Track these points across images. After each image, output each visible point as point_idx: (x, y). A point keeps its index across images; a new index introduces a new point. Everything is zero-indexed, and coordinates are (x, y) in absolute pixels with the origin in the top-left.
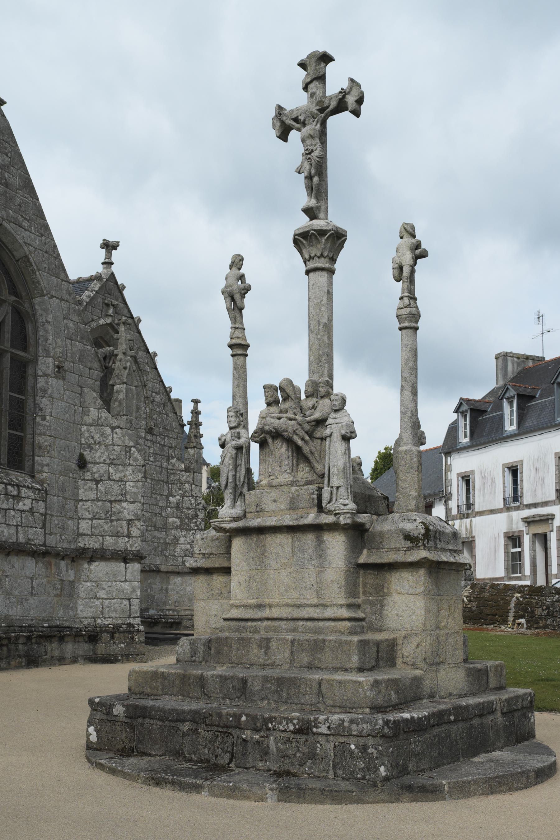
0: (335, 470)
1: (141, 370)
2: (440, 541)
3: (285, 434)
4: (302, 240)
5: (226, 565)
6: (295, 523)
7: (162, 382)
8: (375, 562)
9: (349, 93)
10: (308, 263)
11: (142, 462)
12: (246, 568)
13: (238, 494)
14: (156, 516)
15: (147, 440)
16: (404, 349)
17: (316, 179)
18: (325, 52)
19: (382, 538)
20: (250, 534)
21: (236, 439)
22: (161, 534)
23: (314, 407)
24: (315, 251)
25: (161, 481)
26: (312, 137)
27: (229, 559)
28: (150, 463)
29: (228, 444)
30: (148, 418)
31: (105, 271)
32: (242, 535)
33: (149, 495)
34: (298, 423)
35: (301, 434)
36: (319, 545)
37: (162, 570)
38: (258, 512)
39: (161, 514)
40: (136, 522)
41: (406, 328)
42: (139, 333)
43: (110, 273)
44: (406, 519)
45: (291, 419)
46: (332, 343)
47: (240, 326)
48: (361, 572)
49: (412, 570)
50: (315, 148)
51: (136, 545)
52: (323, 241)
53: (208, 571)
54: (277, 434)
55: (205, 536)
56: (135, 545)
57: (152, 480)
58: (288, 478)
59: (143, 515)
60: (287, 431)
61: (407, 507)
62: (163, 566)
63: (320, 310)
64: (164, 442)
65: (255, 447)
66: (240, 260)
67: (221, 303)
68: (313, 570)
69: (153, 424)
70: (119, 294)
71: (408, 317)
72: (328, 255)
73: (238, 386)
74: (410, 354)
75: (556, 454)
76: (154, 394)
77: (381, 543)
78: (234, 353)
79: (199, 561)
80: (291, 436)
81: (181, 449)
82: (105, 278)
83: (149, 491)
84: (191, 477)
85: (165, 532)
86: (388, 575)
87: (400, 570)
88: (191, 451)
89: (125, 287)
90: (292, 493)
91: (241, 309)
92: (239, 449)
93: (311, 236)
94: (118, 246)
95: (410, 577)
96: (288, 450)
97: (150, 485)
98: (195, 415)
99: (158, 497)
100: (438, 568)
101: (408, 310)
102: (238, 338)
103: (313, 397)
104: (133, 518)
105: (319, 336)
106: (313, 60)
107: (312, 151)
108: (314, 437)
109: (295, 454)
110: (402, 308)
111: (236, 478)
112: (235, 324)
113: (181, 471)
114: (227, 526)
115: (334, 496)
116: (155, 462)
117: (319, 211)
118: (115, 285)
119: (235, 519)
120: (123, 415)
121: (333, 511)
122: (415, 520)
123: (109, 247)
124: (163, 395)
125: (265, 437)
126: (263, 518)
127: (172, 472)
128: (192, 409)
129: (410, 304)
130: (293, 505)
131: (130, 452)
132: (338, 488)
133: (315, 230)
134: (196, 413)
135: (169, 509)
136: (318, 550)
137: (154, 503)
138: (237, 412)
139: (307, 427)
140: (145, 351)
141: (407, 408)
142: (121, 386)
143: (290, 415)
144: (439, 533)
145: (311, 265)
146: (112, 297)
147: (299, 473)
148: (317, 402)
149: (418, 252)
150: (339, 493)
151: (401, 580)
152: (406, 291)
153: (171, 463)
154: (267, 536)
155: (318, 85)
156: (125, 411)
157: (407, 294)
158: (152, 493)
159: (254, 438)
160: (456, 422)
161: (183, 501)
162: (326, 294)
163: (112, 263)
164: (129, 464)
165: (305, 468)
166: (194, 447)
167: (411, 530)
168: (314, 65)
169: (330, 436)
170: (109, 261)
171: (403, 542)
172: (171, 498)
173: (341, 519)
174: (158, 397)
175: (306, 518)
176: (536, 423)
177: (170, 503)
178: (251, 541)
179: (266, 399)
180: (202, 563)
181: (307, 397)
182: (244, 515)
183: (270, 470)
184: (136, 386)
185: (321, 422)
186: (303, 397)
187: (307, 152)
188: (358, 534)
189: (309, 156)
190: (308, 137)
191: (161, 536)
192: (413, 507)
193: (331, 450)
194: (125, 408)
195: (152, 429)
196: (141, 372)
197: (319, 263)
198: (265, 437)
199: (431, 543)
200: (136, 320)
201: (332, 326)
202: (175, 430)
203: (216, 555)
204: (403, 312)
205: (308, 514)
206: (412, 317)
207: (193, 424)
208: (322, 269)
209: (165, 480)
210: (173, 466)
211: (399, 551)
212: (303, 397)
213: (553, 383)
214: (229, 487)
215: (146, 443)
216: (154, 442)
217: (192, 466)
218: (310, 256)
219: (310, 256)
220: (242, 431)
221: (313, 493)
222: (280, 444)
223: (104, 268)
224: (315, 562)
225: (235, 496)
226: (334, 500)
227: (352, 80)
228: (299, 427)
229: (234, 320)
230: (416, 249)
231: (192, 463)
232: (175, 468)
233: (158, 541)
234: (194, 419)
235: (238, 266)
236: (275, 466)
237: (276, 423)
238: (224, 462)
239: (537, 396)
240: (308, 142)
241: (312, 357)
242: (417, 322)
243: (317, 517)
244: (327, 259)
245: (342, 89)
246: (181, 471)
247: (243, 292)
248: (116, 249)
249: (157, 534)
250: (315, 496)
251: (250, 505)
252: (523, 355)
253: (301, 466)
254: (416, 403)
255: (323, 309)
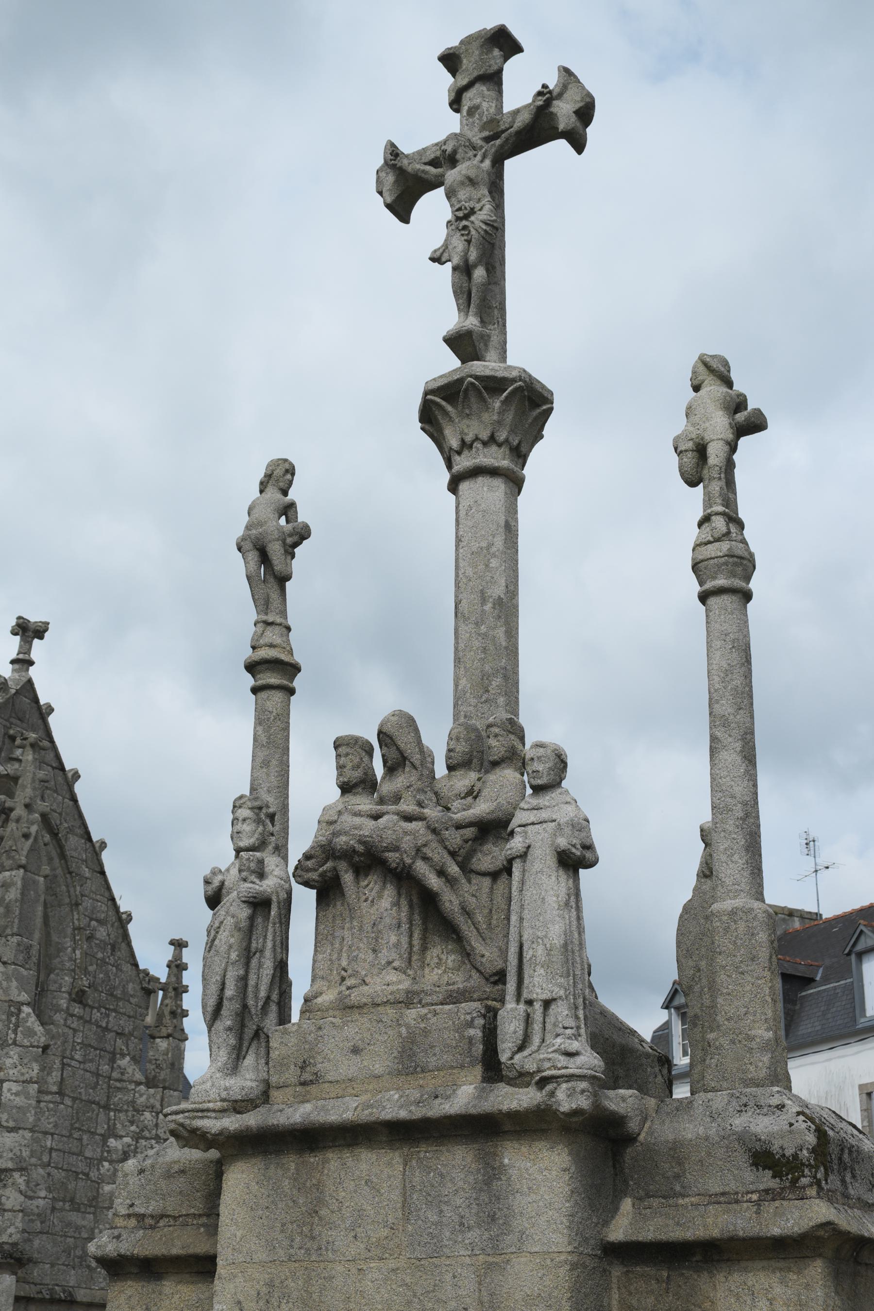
0: (540, 951)
1: (70, 873)
2: (854, 1177)
3: (392, 857)
4: (443, 403)
5: (201, 1248)
6: (418, 1113)
7: (113, 900)
8: (663, 1237)
9: (560, 96)
10: (456, 458)
11: (43, 1039)
12: (261, 1256)
13: (249, 1032)
14: (77, 1178)
15: (72, 1015)
16: (718, 643)
17: (479, 273)
18: (503, 26)
19: (680, 1164)
20: (279, 1152)
21: (253, 878)
22: (84, 1219)
23: (472, 793)
24: (476, 428)
25: (94, 1102)
26: (471, 182)
27: (213, 1230)
28: (73, 1063)
29: (228, 893)
30: (77, 971)
31: (16, 676)
32: (253, 1155)
33: (64, 1132)
34: (428, 827)
35: (436, 858)
36: (488, 1183)
37: (79, 1299)
38: (303, 1084)
39: (87, 1175)
40: (16, 1175)
41: (720, 591)
42: (74, 799)
43: (24, 680)
44: (751, 1104)
45: (408, 818)
46: (517, 649)
47: (279, 620)
48: (617, 1272)
49: (782, 1264)
50: (478, 206)
51: (12, 1230)
52: (497, 404)
53: (149, 1268)
54: (369, 860)
55: (149, 1162)
56: (9, 1231)
57: (74, 1099)
58: (396, 982)
59: (49, 1174)
60: (396, 849)
61: (744, 1072)
62: (82, 1292)
63: (487, 566)
64: (107, 1023)
65: (305, 900)
66: (287, 471)
67: (236, 568)
68: (468, 1260)
69: (86, 983)
70: (40, 721)
71: (726, 564)
72: (507, 441)
73: (266, 764)
74: (735, 655)
75: (861, 1087)
76: (94, 923)
77: (677, 1177)
78: (260, 682)
79: (124, 1237)
80: (408, 861)
81: (141, 1039)
82: (13, 688)
83: (67, 1123)
84: (158, 1097)
85: (94, 1213)
86: (703, 1281)
87: (743, 1264)
88: (162, 1044)
89: (53, 710)
90: (408, 1026)
91: (282, 580)
92: (259, 905)
93: (466, 390)
94: (46, 630)
95: (778, 1290)
96: (397, 904)
97: (70, 1110)
98: (175, 970)
99: (85, 1137)
100: (857, 1262)
101: (725, 546)
102: (272, 646)
103: (470, 769)
104: (10, 1165)
105: (483, 629)
106: (476, 44)
107: (472, 212)
108: (472, 871)
109: (416, 917)
110: (709, 542)
111: (246, 986)
112: (266, 614)
113: (139, 1084)
114: (212, 1125)
115: (537, 1027)
116: (84, 1063)
117: (486, 345)
118: (34, 705)
119: (238, 1106)
120: (12, 935)
121: (531, 1075)
122: (781, 1107)
123: (29, 631)
124: (112, 926)
125: (335, 871)
126: (320, 1103)
127: (118, 1085)
128: (170, 958)
129: (729, 533)
130: (409, 1062)
131: (18, 1015)
132: (547, 1004)
133: (477, 378)
134: (177, 966)
135: (106, 1164)
136: (484, 1197)
137: (75, 1150)
138: (260, 808)
139: (455, 838)
140: (82, 837)
141: (733, 797)
142: (14, 873)
143: (408, 806)
144: (850, 1152)
145: (463, 462)
146: (25, 725)
147: (427, 970)
148: (479, 779)
149: (740, 417)
150: (550, 1020)
151: (748, 1299)
152: (719, 501)
153: (119, 1067)
154: (330, 1155)
155: (486, 93)
156: (16, 926)
157: (720, 509)
158: (72, 1127)
159: (302, 875)
160: (667, 1026)
161: (136, 1148)
162: (502, 530)
163: (31, 663)
164: (15, 1043)
165: (444, 957)
166: (168, 1036)
167: (772, 1135)
168: (477, 53)
169: (523, 856)
170: (26, 657)
171: (749, 1175)
172: (112, 1140)
173: (561, 1095)
174: (102, 929)
175: (448, 1097)
176: (819, 1028)
177: (109, 1152)
178: (280, 1172)
179: (340, 775)
180: (133, 1243)
181: (450, 768)
182: (265, 1096)
183: (344, 963)
184: (46, 877)
185: (494, 828)
186: (440, 770)
187: (460, 214)
188: (605, 1147)
189: (464, 223)
190: (462, 183)
191: (84, 1223)
192: (763, 1073)
193: (527, 894)
194: (16, 921)
195: (83, 992)
196: (72, 877)
197: (485, 457)
198: (335, 869)
199: (834, 1181)
200: (70, 775)
201: (516, 607)
202: (132, 1000)
203: (175, 1218)
204: (711, 550)
205: (456, 1085)
206: (735, 564)
207: (170, 990)
208: (493, 472)
209: (102, 1103)
210: (122, 1074)
211: (737, 1202)
212: (440, 770)
213: (849, 954)
214: (224, 1012)
215: (69, 1022)
216: (86, 1022)
217: (162, 1076)
218: (463, 441)
219: (463, 441)
220: (271, 862)
221: (470, 1024)
222: (377, 888)
223: (13, 670)
224: (473, 1235)
225: (240, 1039)
226: (536, 1040)
227: (566, 72)
228: (431, 837)
229: (263, 604)
230: (736, 412)
231: (161, 1069)
232: (125, 1077)
233: (77, 1235)
234: (173, 979)
235: (281, 484)
236: (358, 948)
237: (368, 827)
238: (217, 942)
239: (818, 978)
240: (463, 194)
241: (463, 682)
242: (748, 578)
243: (481, 1094)
244: (505, 449)
245: (544, 86)
246: (139, 1084)
247: (289, 541)
248: (41, 637)
249: (75, 1217)
250: (476, 1033)
251: (283, 1065)
252: (783, 908)
253: (434, 952)
254: (755, 786)
255: (494, 563)
